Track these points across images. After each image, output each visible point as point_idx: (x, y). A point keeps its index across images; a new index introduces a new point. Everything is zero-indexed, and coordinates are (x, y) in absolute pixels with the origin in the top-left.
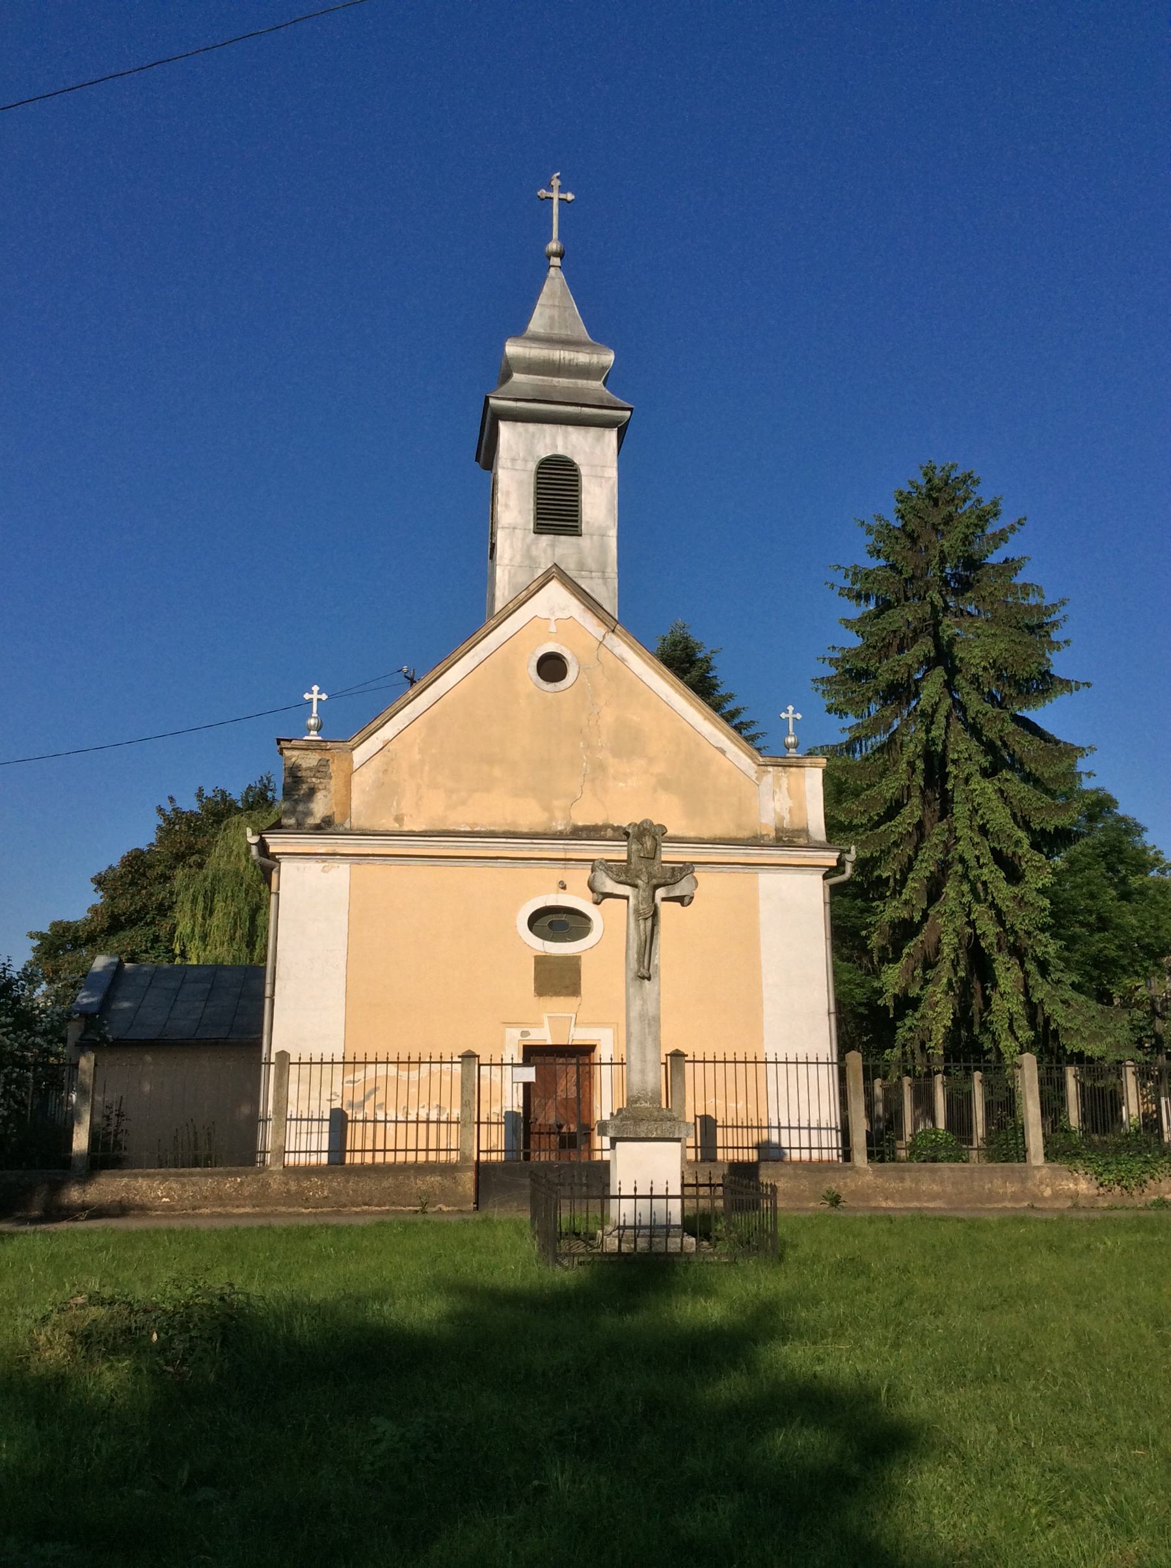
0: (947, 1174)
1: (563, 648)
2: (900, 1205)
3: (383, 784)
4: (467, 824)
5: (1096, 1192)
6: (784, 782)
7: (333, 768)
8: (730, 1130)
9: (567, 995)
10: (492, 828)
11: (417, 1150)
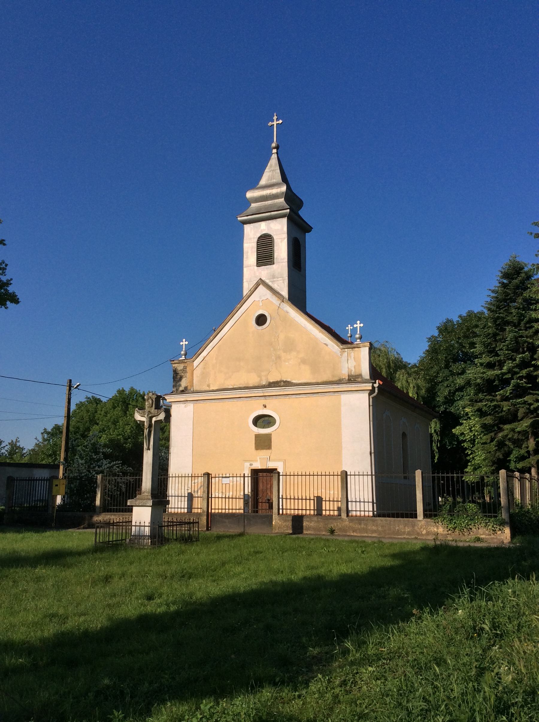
0: (379, 522)
1: (265, 311)
2: (359, 535)
4: (232, 385)
5: (447, 533)
6: (352, 354)
7: (188, 369)
8: (237, 499)
9: (267, 449)
10: (240, 386)
11: (360, 511)
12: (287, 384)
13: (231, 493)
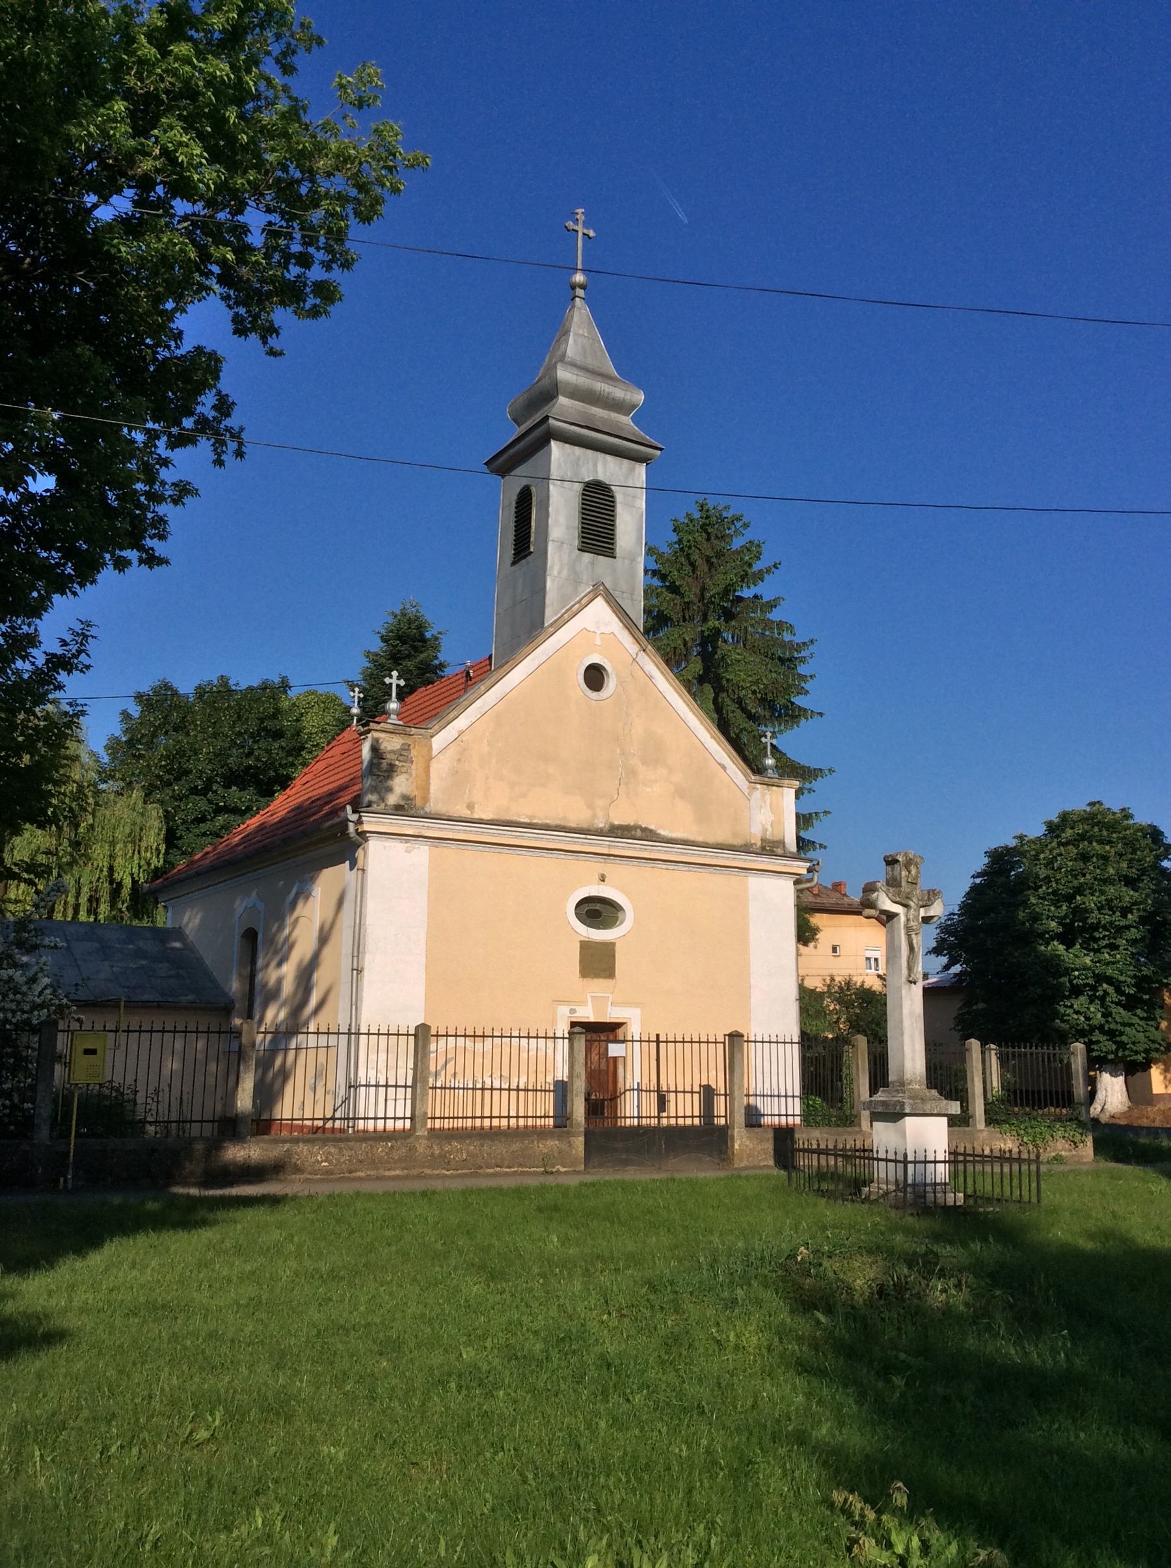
1: (606, 661)
3: (457, 772)
4: (528, 816)
8: (539, 1093)
9: (605, 977)
10: (548, 822)
11: (376, 1118)
12: (649, 835)
13: (523, 1080)
